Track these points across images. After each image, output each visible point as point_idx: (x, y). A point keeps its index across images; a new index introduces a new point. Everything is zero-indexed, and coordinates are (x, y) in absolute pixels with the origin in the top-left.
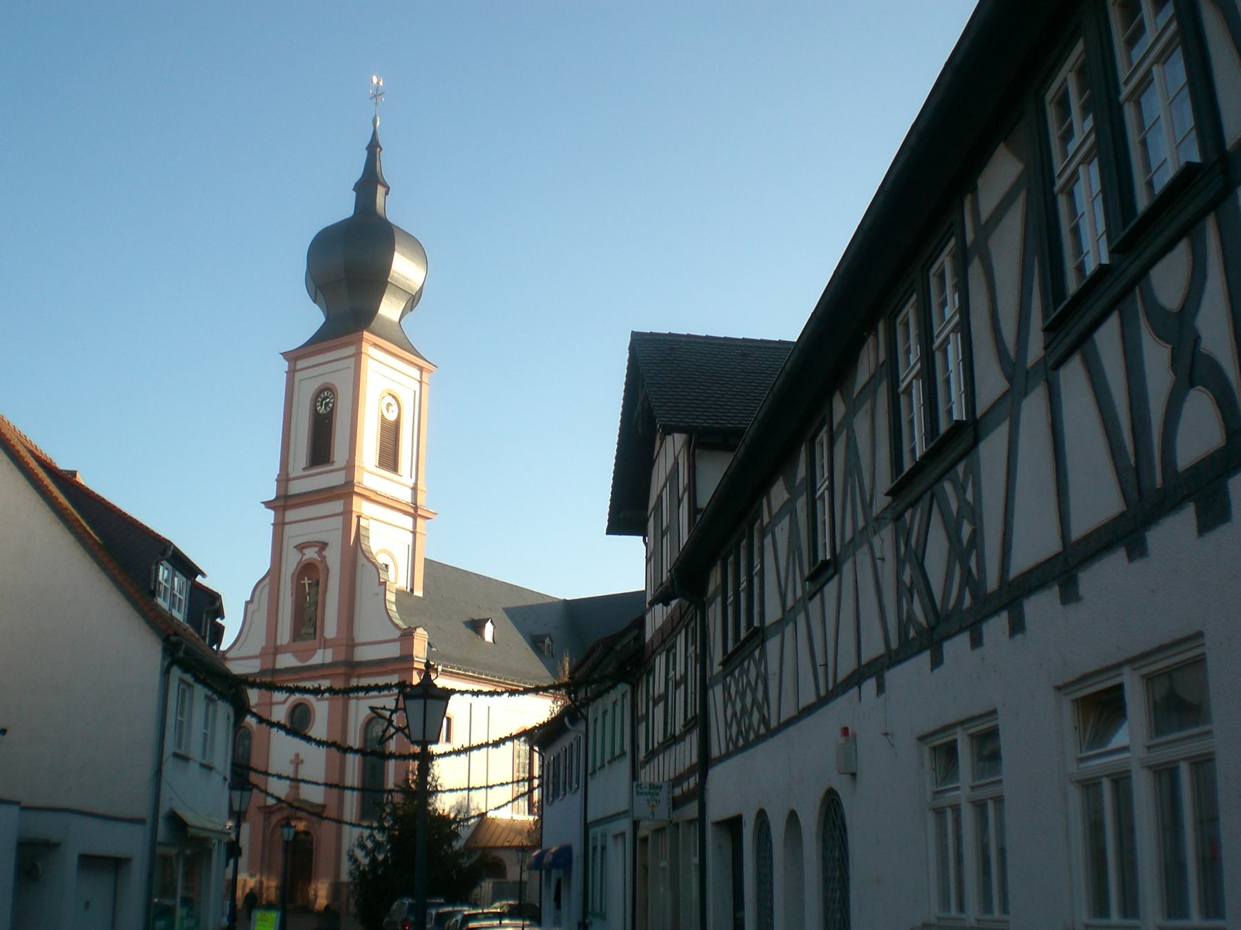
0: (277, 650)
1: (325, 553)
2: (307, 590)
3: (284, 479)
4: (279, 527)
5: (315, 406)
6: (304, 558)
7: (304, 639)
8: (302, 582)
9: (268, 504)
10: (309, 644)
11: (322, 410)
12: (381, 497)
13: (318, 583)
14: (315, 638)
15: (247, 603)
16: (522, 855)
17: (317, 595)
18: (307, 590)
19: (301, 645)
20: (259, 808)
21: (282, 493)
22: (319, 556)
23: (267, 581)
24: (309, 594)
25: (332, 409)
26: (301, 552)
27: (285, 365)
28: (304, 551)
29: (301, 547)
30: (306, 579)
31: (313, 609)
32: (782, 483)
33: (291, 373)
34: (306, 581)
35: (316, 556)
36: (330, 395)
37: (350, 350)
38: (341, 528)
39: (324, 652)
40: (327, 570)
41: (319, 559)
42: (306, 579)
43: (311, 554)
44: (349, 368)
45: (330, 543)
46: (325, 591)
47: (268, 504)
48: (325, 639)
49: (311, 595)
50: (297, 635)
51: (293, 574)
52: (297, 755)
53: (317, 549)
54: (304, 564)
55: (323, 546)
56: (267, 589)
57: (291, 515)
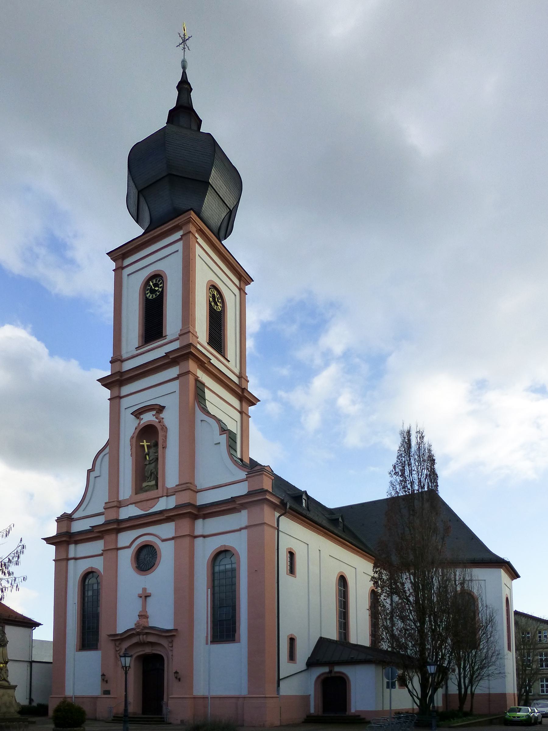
0: (119, 505)
1: (162, 416)
2: (146, 451)
3: (116, 360)
4: (115, 400)
5: (145, 294)
6: (142, 422)
7: (146, 491)
8: (141, 444)
9: (49, 540)
10: (152, 494)
11: (150, 296)
12: (215, 369)
13: (156, 445)
14: (157, 489)
15: (89, 471)
16: (392, 669)
17: (157, 452)
18: (146, 451)
19: (143, 496)
20: (110, 636)
21: (64, 530)
22: (156, 418)
23: (107, 450)
24: (148, 454)
25: (162, 293)
26: (138, 418)
27: (113, 265)
28: (142, 417)
29: (138, 414)
30: (145, 441)
31: (153, 465)
32: (182, 242)
33: (118, 270)
34: (145, 443)
35: (154, 418)
36: (159, 281)
37: (177, 235)
38: (178, 392)
39: (167, 502)
40: (165, 429)
41: (157, 421)
42: (145, 441)
43: (148, 418)
44: (178, 251)
45: (180, 682)
46: (164, 448)
47: (49, 540)
48: (167, 489)
49: (150, 455)
50: (139, 489)
51: (132, 438)
52: (144, 589)
53: (154, 412)
54: (141, 428)
55: (160, 409)
56: (107, 458)
57: (126, 390)
